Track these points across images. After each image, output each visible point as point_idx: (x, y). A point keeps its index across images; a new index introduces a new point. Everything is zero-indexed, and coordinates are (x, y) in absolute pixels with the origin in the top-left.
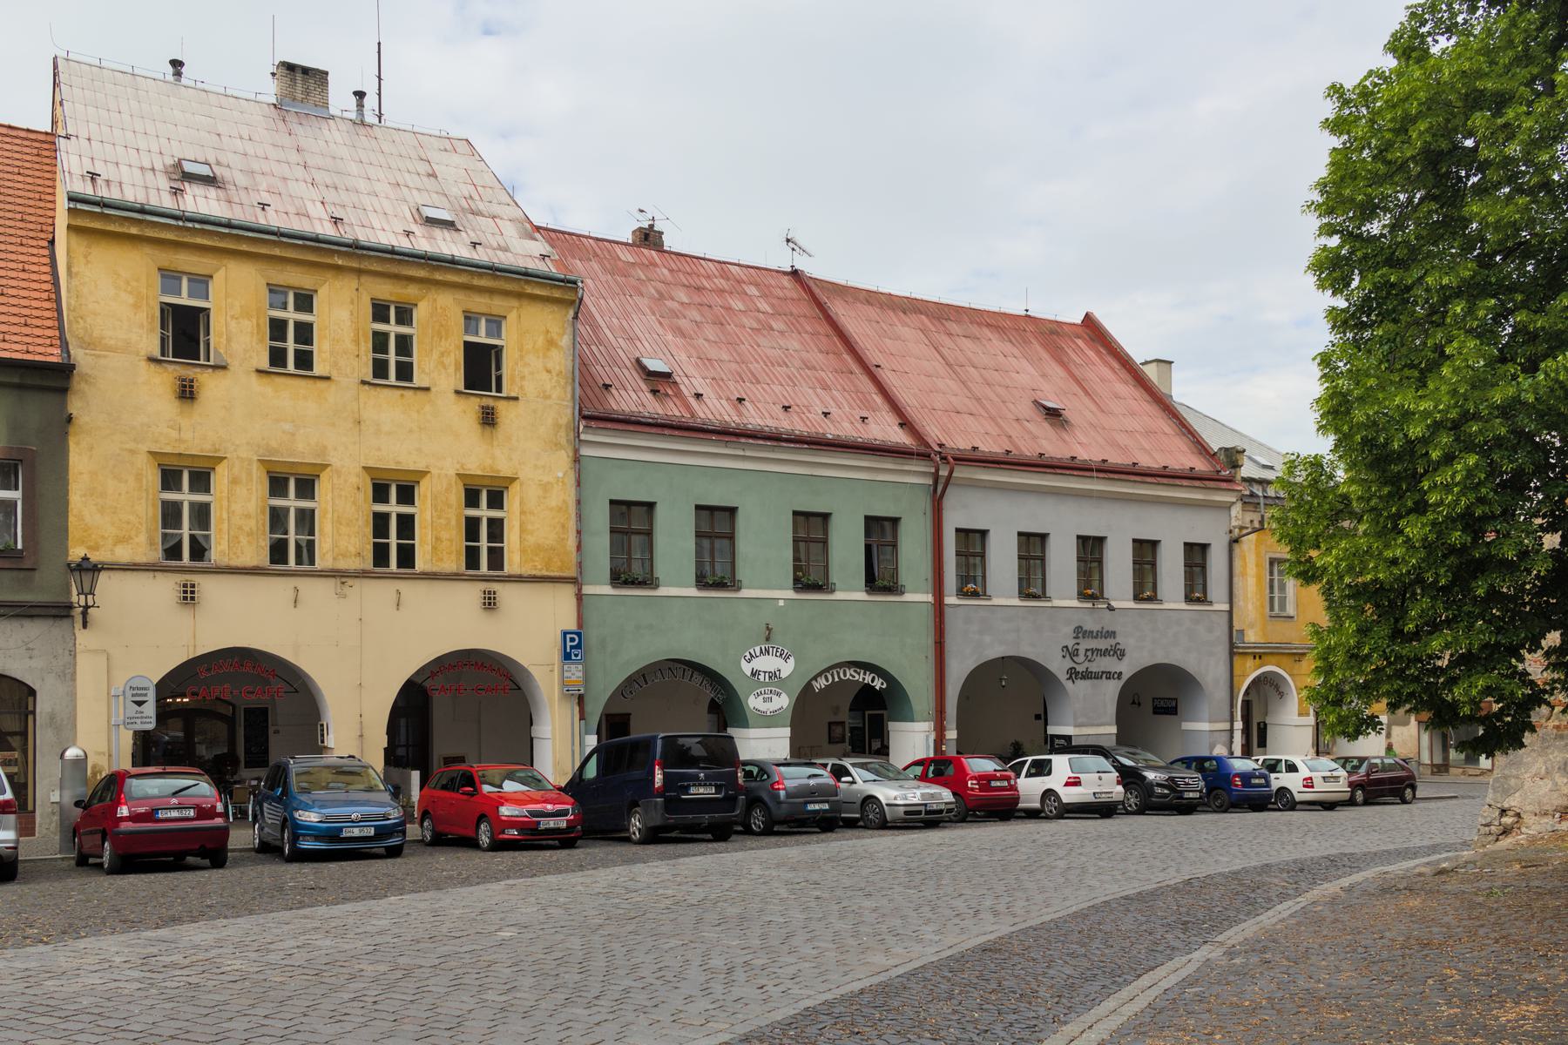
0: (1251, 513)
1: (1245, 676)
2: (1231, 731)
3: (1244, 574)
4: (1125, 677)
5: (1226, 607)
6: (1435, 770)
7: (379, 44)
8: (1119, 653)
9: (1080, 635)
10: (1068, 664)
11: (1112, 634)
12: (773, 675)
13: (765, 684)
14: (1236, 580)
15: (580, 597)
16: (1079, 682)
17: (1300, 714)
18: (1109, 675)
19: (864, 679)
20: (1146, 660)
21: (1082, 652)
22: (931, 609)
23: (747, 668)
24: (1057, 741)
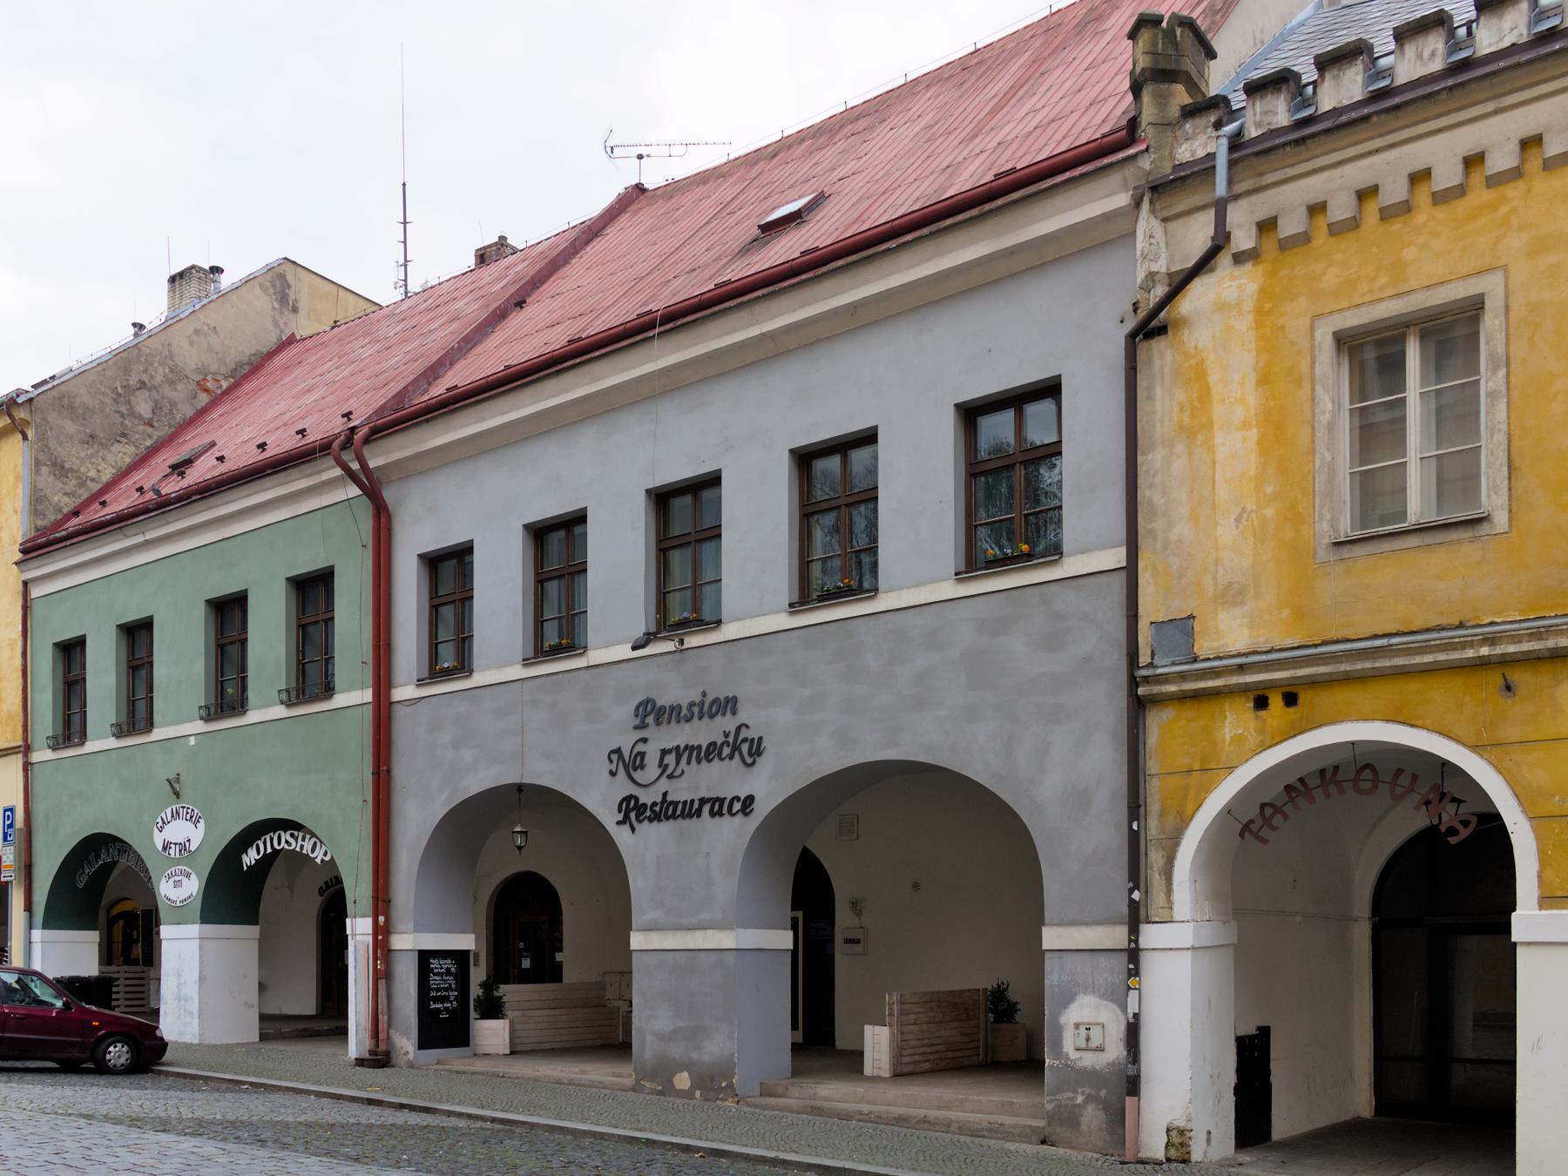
1: (1210, 769)
3: (1197, 427)
4: (762, 809)
7: (404, 185)
8: (747, 749)
9: (650, 720)
10: (623, 788)
11: (729, 705)
12: (183, 847)
13: (177, 862)
15: (27, 766)
16: (646, 828)
18: (717, 807)
19: (302, 846)
20: (827, 758)
21: (652, 760)
22: (368, 713)
23: (158, 839)
24: (434, 964)
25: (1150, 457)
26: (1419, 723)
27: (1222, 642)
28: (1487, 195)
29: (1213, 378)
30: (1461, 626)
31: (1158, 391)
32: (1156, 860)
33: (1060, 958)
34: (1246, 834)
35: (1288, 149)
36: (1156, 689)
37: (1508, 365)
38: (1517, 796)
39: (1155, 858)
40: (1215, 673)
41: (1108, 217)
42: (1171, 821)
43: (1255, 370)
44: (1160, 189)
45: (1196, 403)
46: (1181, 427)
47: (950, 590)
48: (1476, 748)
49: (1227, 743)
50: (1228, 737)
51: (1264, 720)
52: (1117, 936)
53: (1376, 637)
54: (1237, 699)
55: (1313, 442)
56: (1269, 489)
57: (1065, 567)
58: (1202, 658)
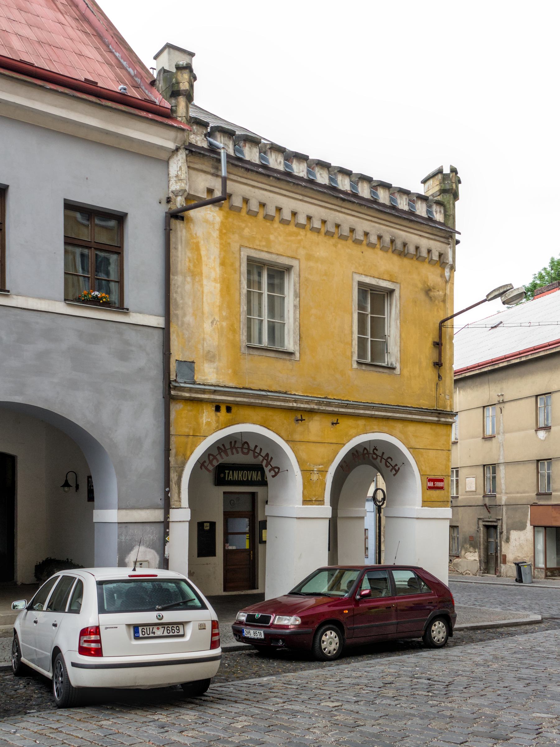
0: (209, 177)
2: (166, 524)
5: (159, 322)
6: (549, 574)
14: (177, 280)
17: (306, 502)
25: (176, 278)
26: (271, 428)
27: (205, 378)
28: (295, 229)
29: (203, 253)
30: (285, 393)
31: (180, 247)
32: (173, 477)
33: (126, 527)
34: (203, 467)
35: (243, 170)
36: (180, 393)
37: (299, 297)
38: (298, 462)
39: (173, 476)
40: (204, 391)
41: (161, 148)
42: (180, 458)
43: (219, 257)
44: (193, 153)
45: (195, 261)
46: (189, 269)
47: (61, 307)
48: (287, 441)
49: (204, 425)
50: (204, 421)
51: (218, 417)
52: (157, 515)
53: (260, 390)
54: (209, 405)
55: (240, 299)
56: (224, 314)
57: (131, 317)
58: (197, 383)
